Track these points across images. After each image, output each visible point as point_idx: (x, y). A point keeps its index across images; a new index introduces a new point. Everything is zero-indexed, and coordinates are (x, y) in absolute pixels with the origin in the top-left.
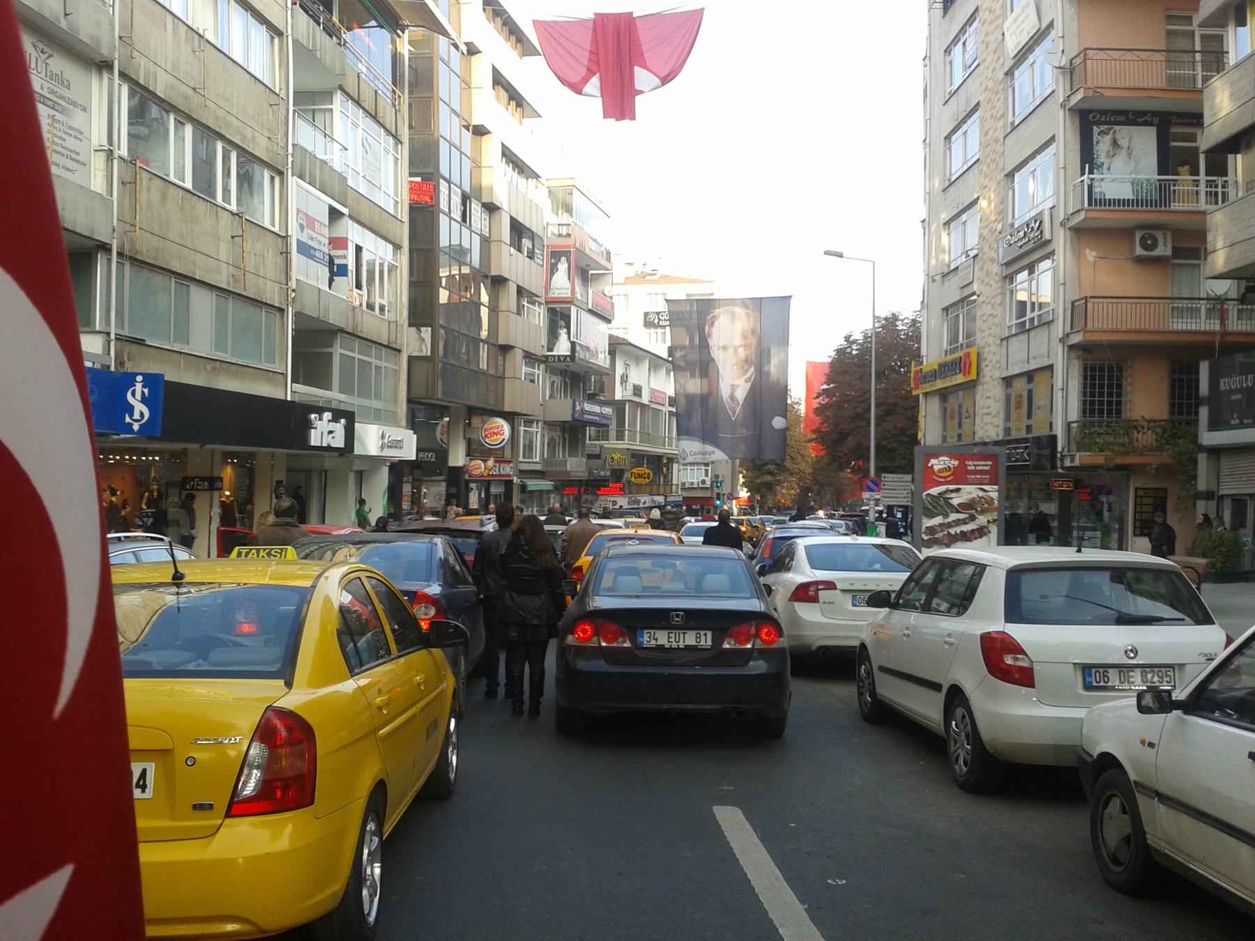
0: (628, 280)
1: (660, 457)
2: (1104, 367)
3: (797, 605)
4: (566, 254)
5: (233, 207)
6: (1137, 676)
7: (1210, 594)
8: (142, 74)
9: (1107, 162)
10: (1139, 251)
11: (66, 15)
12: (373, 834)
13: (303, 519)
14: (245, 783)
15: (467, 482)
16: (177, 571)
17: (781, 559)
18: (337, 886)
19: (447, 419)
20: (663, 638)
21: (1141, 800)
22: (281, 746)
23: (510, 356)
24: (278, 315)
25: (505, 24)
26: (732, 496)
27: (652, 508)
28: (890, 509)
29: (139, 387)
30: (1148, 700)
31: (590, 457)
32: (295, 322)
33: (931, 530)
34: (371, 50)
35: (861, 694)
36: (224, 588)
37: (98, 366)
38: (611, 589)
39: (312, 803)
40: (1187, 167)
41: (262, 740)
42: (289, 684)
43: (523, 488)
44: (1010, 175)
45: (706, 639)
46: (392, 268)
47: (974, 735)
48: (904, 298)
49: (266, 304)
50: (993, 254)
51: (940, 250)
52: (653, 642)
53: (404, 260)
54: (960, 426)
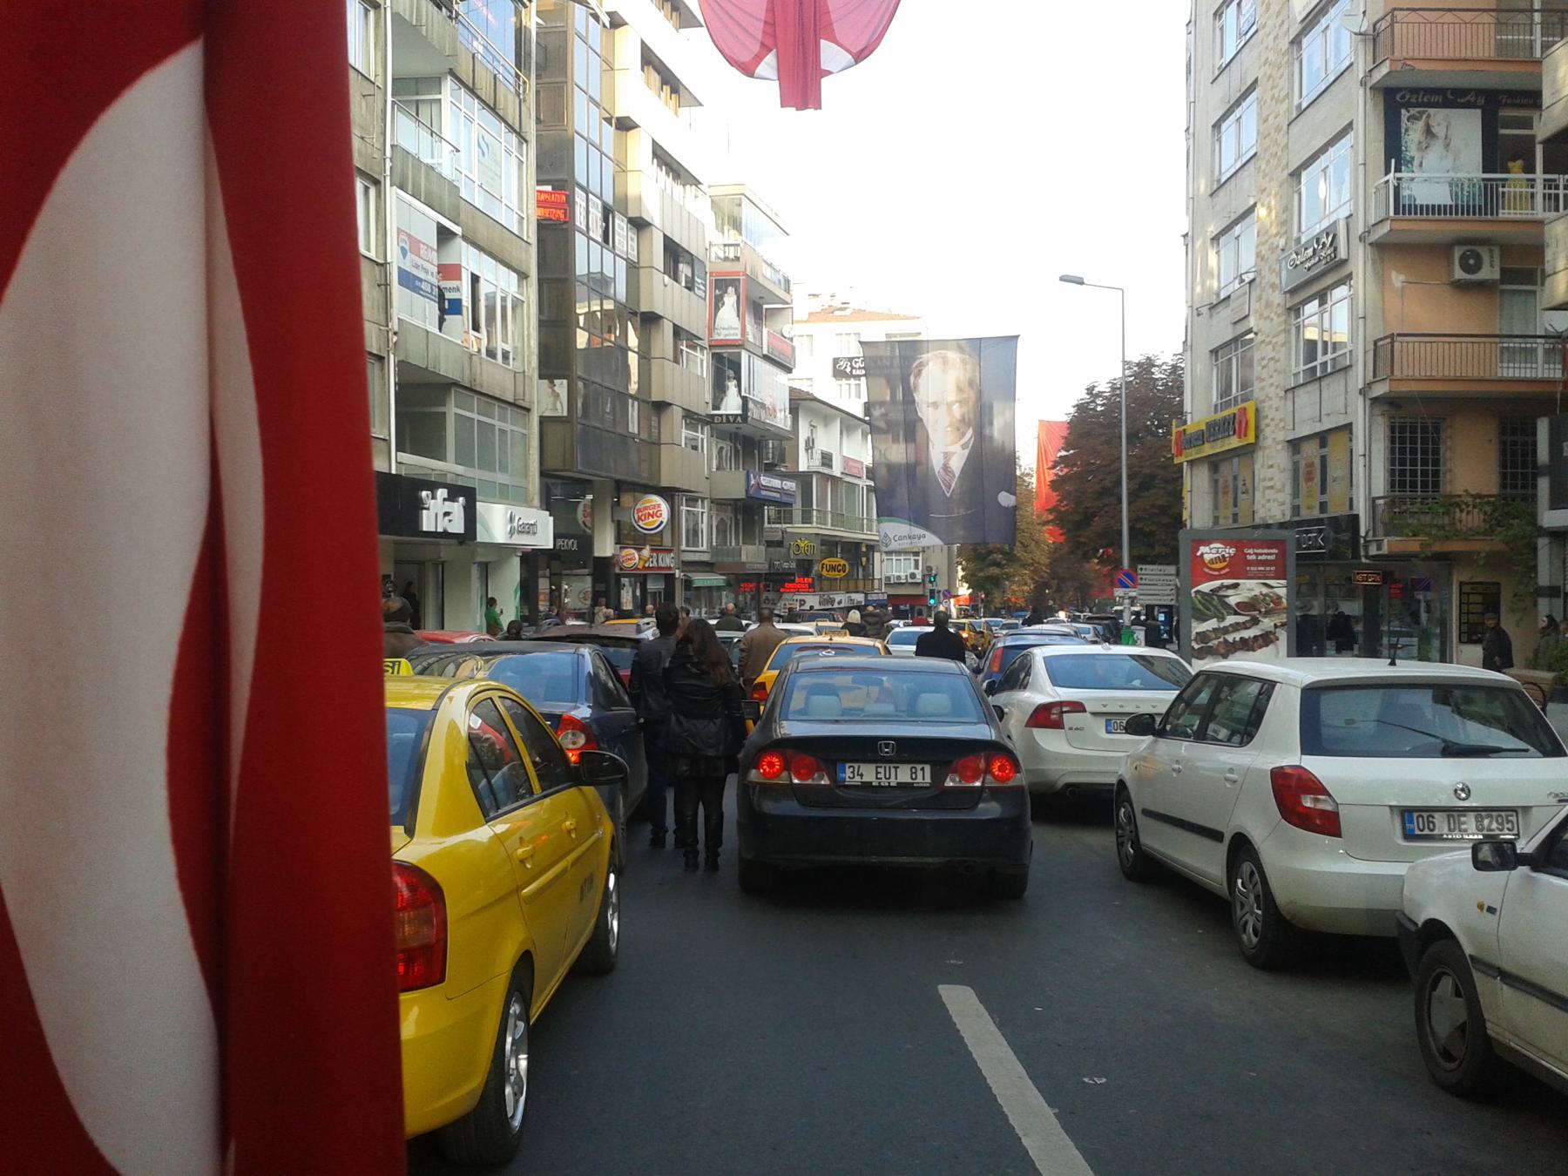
2: (1416, 426)
10: (1459, 274)
33: (1203, 637)
40: (1519, 163)
44: (1296, 174)
47: (1266, 898)
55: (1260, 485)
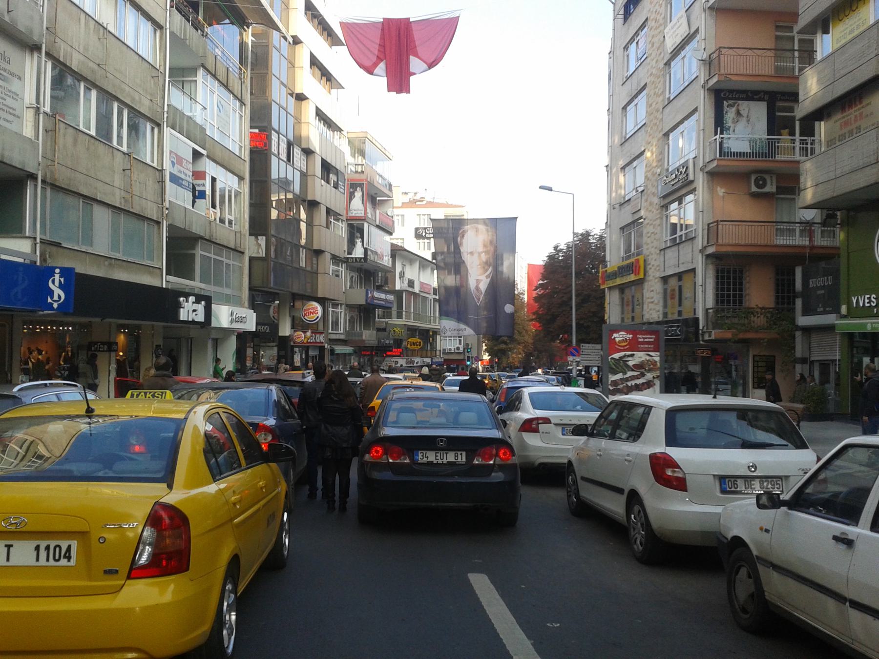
0: (404, 205)
1: (427, 331)
2: (730, 269)
3: (525, 435)
4: (361, 186)
5: (124, 149)
6: (756, 484)
7: (806, 429)
8: (62, 54)
9: (732, 126)
10: (754, 189)
11: (9, 12)
12: (231, 592)
13: (176, 372)
14: (141, 555)
15: (293, 347)
16: (89, 407)
17: (512, 402)
18: (206, 628)
19: (277, 302)
20: (431, 456)
21: (760, 568)
22: (165, 530)
23: (321, 258)
24: (156, 226)
25: (320, 23)
26: (478, 359)
27: (422, 366)
28: (587, 368)
29: (57, 277)
30: (764, 500)
31: (379, 330)
32: (169, 231)
33: (615, 383)
34: (225, 40)
35: (569, 496)
36: (121, 419)
37: (27, 262)
38: (394, 422)
39: (187, 569)
40: (787, 130)
41: (152, 526)
42: (170, 487)
43: (332, 351)
44: (667, 135)
45: (462, 458)
46: (237, 194)
47: (647, 525)
48: (594, 219)
49: (62, 188)
50: (654, 190)
51: (619, 186)
52: (425, 459)
53: (246, 189)
54: (633, 312)
55: (646, 301)
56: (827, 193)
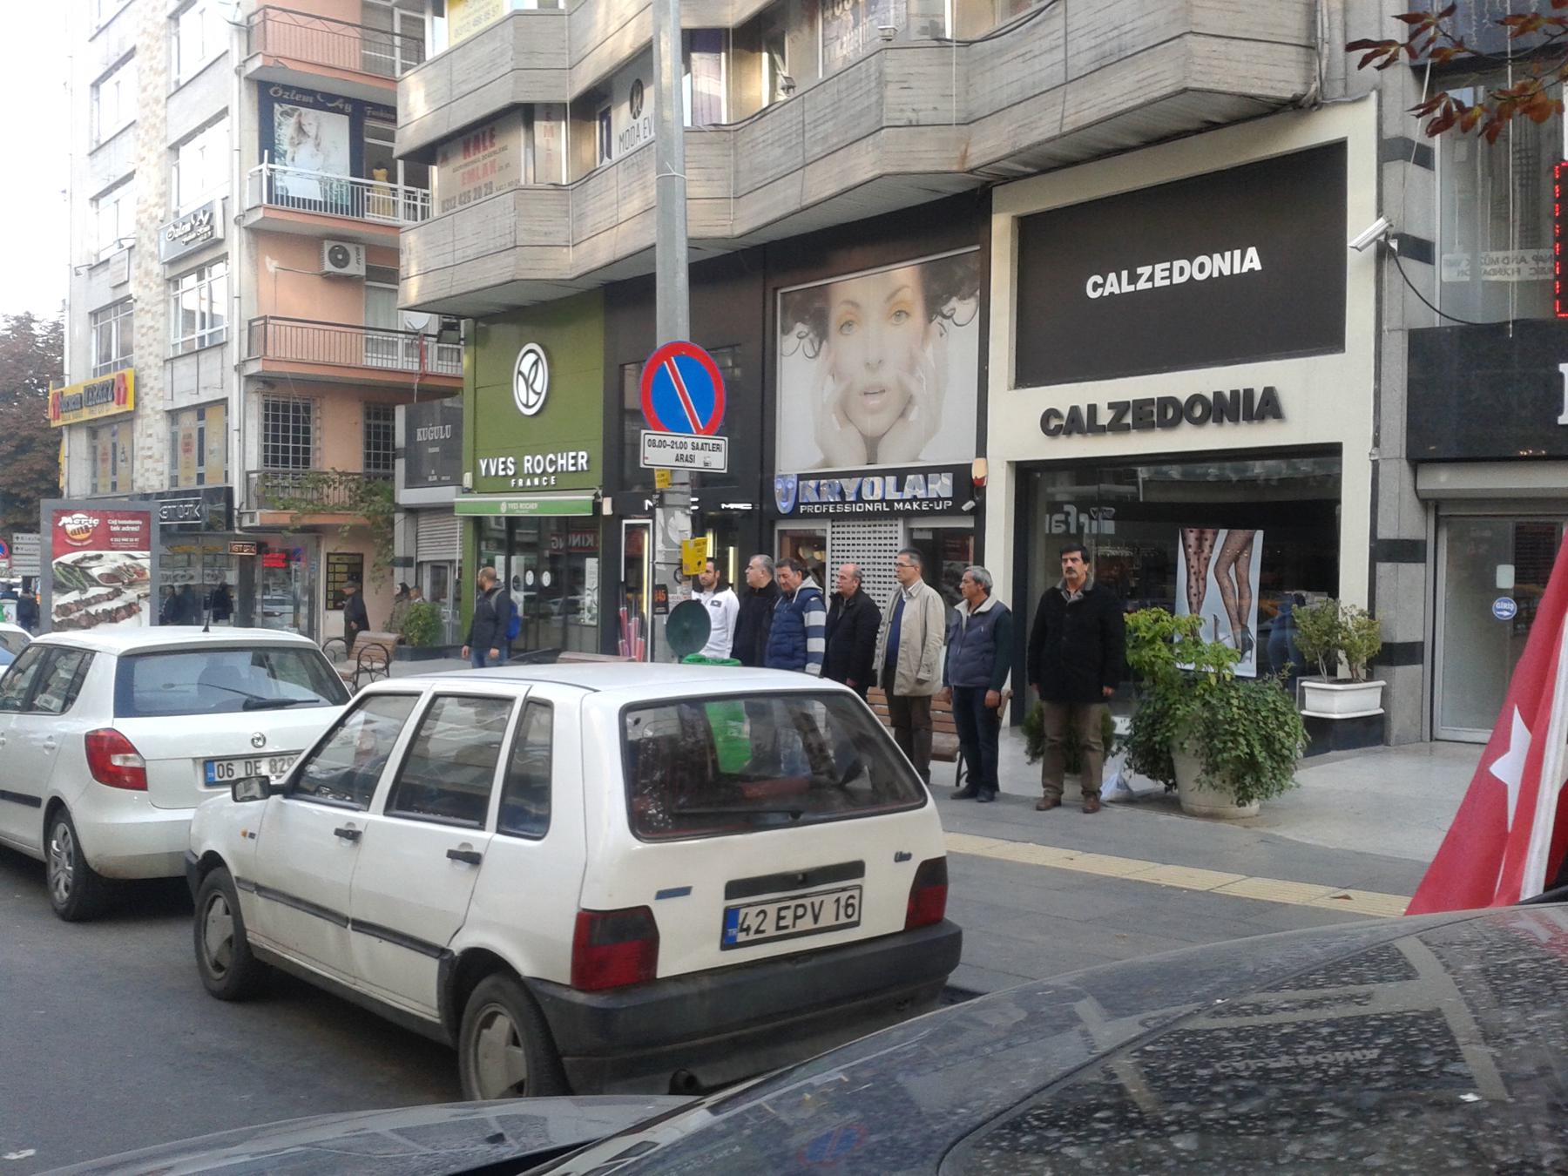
2: (288, 409)
10: (328, 267)
21: (241, 894)
33: (65, 609)
40: (383, 171)
44: (175, 148)
47: (77, 856)
50: (152, 248)
55: (138, 453)
56: (441, 289)
